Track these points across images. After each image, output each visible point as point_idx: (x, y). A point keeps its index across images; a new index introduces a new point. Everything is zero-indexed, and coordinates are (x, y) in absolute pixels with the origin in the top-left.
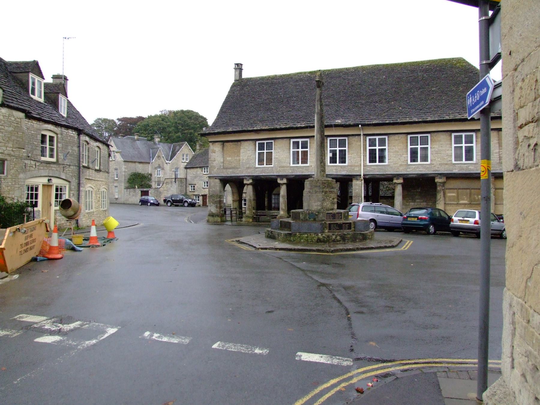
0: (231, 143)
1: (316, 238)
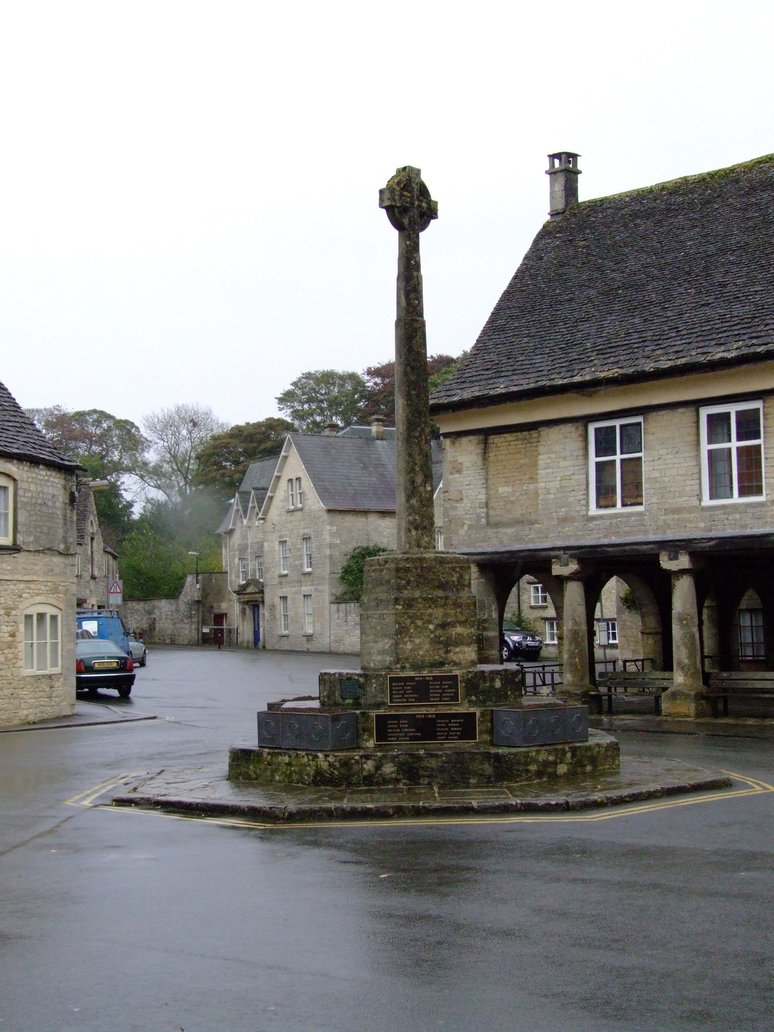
0: (509, 437)
1: (311, 770)
